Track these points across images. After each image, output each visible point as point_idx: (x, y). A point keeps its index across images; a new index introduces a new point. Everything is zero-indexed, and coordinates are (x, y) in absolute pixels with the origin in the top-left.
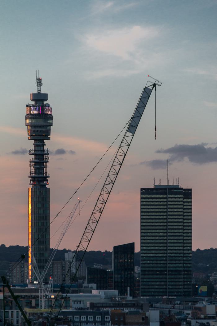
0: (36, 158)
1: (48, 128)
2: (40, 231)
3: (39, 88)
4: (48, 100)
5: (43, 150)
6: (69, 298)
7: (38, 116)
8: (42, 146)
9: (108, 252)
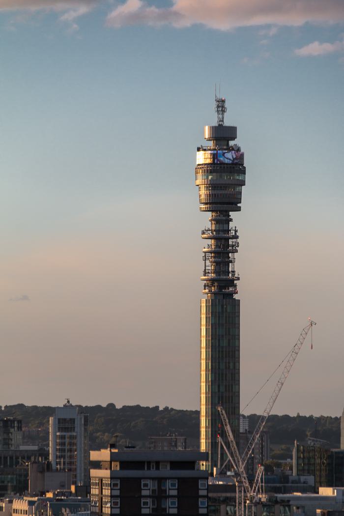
0: (217, 246)
1: (237, 189)
2: (222, 380)
3: (221, 116)
4: (236, 138)
5: (228, 231)
6: (289, 501)
7: (218, 168)
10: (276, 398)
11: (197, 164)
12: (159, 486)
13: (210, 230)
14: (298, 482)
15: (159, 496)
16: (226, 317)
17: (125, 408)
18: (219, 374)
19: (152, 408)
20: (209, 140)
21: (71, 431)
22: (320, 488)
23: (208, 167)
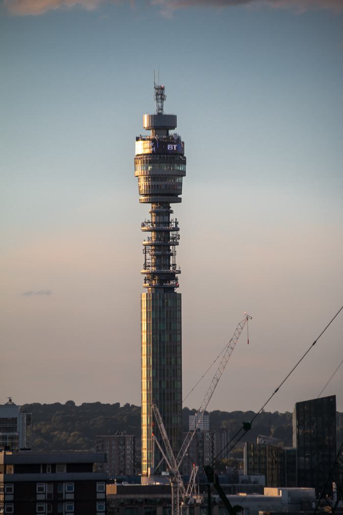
0: (157, 239)
1: (178, 180)
3: (160, 104)
4: (176, 127)
5: (169, 223)
8: (166, 215)
9: (267, 413)
10: (212, 395)
11: (136, 154)
12: (55, 490)
13: (150, 223)
14: (249, 481)
15: (55, 500)
16: (167, 312)
17: (85, 405)
18: (160, 370)
19: (112, 405)
20: (148, 129)
21: (13, 431)
22: (265, 489)
23: (147, 157)
